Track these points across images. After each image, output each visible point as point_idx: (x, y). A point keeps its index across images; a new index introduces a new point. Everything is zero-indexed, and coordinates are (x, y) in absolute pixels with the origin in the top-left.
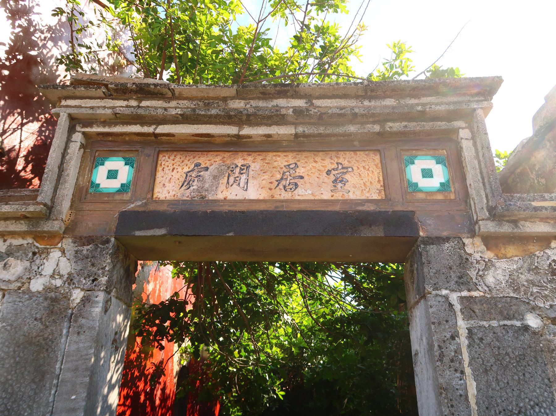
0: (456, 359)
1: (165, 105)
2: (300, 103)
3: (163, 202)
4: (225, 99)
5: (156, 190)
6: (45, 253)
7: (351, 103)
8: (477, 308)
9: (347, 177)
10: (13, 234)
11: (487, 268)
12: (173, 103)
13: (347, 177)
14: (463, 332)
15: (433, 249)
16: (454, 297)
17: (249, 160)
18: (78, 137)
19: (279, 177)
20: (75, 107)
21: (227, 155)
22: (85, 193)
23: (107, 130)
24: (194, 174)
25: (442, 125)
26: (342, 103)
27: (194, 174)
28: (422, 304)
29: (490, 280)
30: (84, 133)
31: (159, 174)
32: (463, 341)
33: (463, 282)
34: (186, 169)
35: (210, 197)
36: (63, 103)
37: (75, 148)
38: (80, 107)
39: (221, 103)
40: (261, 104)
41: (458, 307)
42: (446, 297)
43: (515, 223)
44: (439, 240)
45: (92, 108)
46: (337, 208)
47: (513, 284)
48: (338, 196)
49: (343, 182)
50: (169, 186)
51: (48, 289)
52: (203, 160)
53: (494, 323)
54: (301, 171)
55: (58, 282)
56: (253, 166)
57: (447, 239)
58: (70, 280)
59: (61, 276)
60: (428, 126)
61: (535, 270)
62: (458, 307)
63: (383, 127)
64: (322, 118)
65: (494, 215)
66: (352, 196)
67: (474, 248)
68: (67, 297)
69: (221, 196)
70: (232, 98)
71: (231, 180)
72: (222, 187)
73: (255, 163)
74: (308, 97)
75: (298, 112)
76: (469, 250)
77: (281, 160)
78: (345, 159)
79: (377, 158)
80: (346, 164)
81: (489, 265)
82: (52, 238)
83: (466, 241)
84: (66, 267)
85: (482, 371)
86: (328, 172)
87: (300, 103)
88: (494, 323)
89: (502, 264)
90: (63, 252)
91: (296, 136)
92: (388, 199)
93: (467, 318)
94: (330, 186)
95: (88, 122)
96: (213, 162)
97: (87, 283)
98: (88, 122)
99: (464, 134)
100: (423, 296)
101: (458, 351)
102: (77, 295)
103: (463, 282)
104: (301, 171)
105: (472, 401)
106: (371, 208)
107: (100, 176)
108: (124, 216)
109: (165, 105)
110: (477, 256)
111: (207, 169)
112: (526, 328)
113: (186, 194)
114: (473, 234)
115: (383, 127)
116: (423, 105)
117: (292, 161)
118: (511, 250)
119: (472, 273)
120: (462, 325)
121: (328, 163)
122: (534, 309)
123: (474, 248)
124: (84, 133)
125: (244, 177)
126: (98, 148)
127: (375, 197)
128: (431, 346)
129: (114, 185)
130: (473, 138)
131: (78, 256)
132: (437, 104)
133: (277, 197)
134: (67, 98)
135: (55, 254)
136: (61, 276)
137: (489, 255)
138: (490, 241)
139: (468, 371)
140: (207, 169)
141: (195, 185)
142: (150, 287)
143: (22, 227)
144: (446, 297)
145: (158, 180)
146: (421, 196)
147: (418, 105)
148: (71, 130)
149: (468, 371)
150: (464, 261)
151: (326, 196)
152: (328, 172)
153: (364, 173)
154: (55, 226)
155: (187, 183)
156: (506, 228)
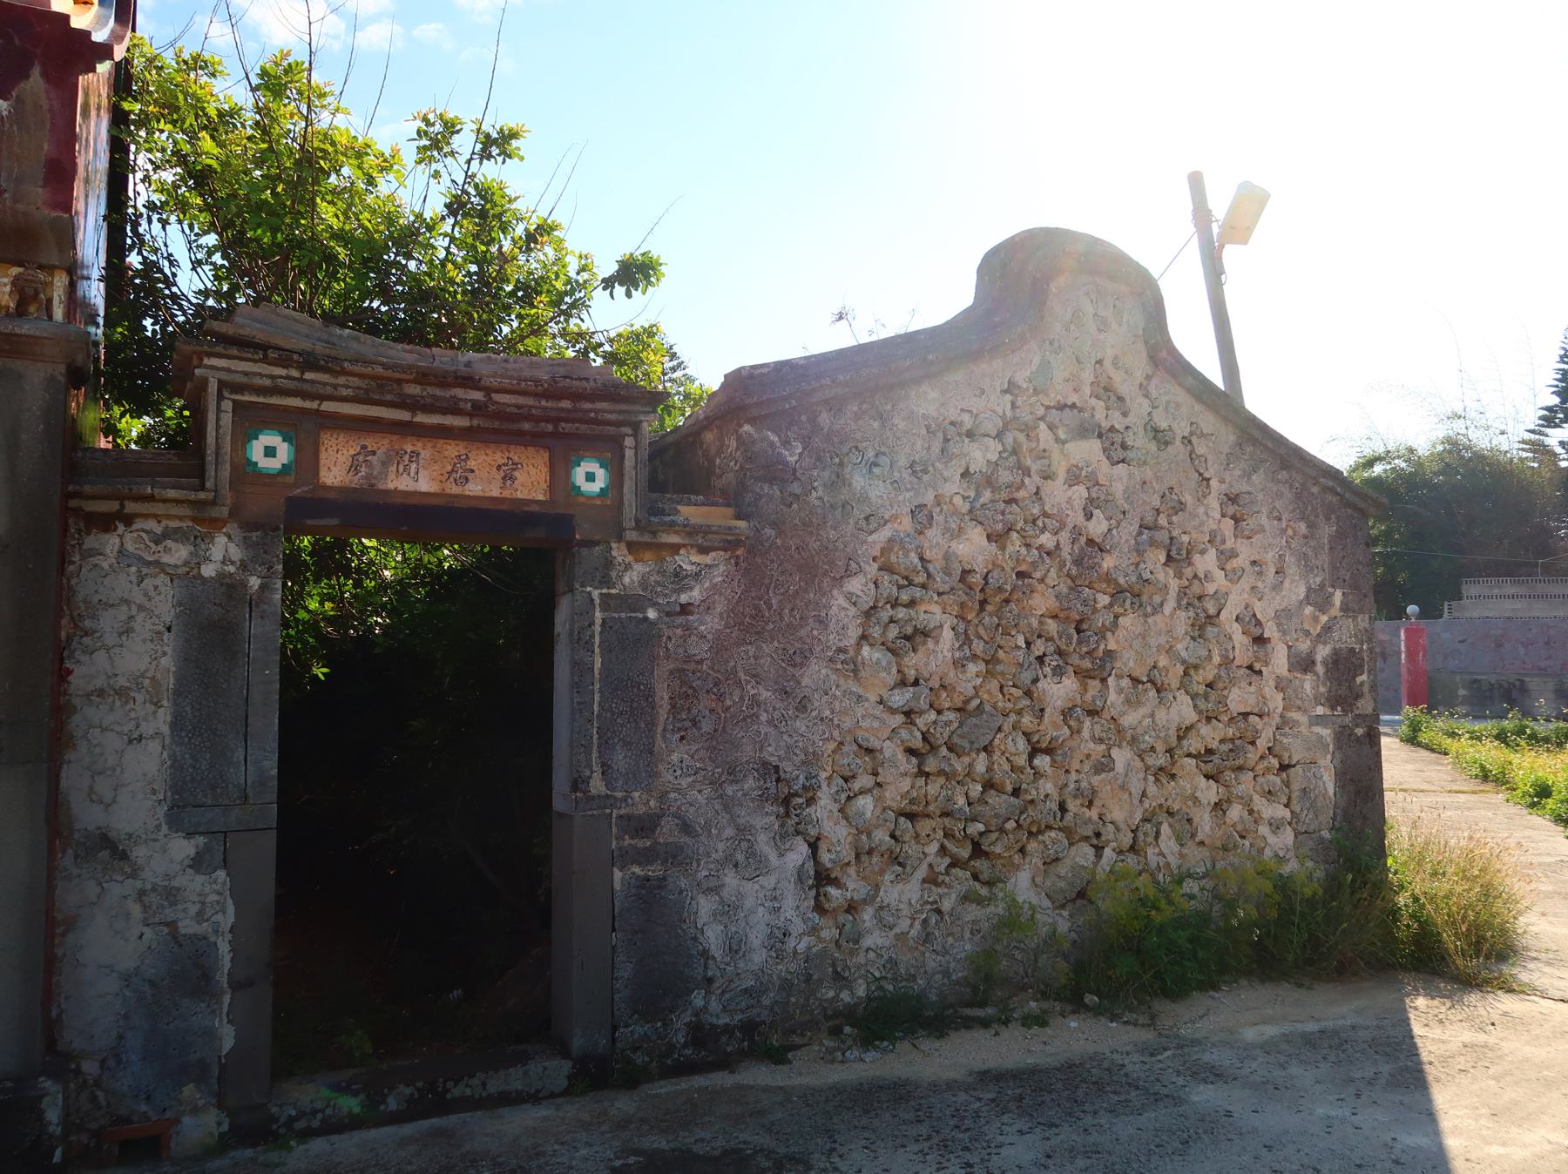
0: (590, 642)
1: (333, 380)
2: (478, 395)
3: (331, 488)
4: (399, 382)
5: (322, 474)
6: (208, 538)
7: (530, 401)
8: (612, 603)
9: (516, 474)
10: (168, 517)
11: (626, 570)
12: (342, 380)
13: (516, 474)
14: (598, 621)
15: (585, 551)
16: (596, 594)
17: (419, 446)
18: (227, 405)
19: (449, 468)
20: (223, 369)
21: (395, 438)
22: (245, 473)
23: (261, 400)
24: (361, 458)
25: (611, 430)
26: (521, 400)
27: (361, 458)
28: (569, 596)
29: (627, 580)
30: (234, 401)
31: (323, 455)
32: (597, 628)
33: (606, 581)
34: (352, 452)
35: (381, 486)
36: (206, 361)
37: (227, 419)
38: (228, 370)
39: (395, 386)
40: (438, 392)
41: (597, 601)
42: (590, 593)
43: (654, 533)
44: (591, 544)
45: (246, 374)
46: (504, 507)
47: (644, 583)
48: (506, 494)
49: (513, 479)
50: (335, 471)
51: (222, 576)
52: (370, 443)
53: (623, 615)
54: (472, 464)
55: (232, 569)
56: (423, 454)
57: (597, 543)
58: (243, 566)
59: (233, 563)
60: (597, 429)
61: (662, 573)
62: (597, 601)
63: (556, 427)
64: (501, 415)
65: (638, 527)
66: (519, 495)
67: (619, 553)
68: (244, 584)
69: (391, 486)
70: (408, 381)
71: (401, 468)
72: (392, 476)
73: (426, 451)
74: (488, 391)
75: (477, 406)
76: (614, 553)
77: (452, 449)
78: (516, 454)
79: (547, 455)
80: (516, 459)
81: (628, 567)
82: (216, 524)
83: (614, 545)
84: (236, 553)
85: (606, 649)
86: (499, 468)
87: (478, 395)
88: (623, 615)
89: (639, 568)
90: (230, 537)
91: (471, 427)
92: (551, 502)
93: (603, 610)
94: (499, 483)
95: (238, 388)
96: (380, 444)
97: (263, 570)
98: (238, 388)
99: (629, 442)
100: (571, 590)
101: (592, 636)
102: (254, 582)
103: (606, 581)
104: (472, 464)
105: (596, 672)
106: (535, 508)
107: (256, 450)
108: (290, 501)
109: (333, 380)
110: (620, 559)
111: (374, 453)
112: (646, 619)
113: (355, 481)
114: (620, 539)
115: (556, 427)
116: (597, 411)
117: (463, 452)
118: (648, 555)
119: (614, 574)
120: (598, 615)
121: (499, 457)
122: (654, 604)
123: (619, 553)
124: (234, 401)
125: (414, 466)
126: (251, 420)
127: (541, 497)
128: (572, 630)
129: (274, 464)
130: (636, 448)
131: (246, 543)
132: (610, 412)
133: (448, 491)
134: (210, 355)
135: (221, 540)
136: (233, 563)
137: (630, 559)
138: (632, 547)
139: (597, 650)
140: (374, 453)
141: (363, 471)
142: (1421, 1002)
143: (185, 511)
144: (590, 593)
145: (322, 462)
146: (582, 500)
147: (591, 411)
148: (220, 397)
149: (597, 650)
150: (609, 563)
151: (495, 493)
152: (499, 468)
153: (533, 471)
154: (215, 512)
155: (354, 468)
156: (647, 538)
